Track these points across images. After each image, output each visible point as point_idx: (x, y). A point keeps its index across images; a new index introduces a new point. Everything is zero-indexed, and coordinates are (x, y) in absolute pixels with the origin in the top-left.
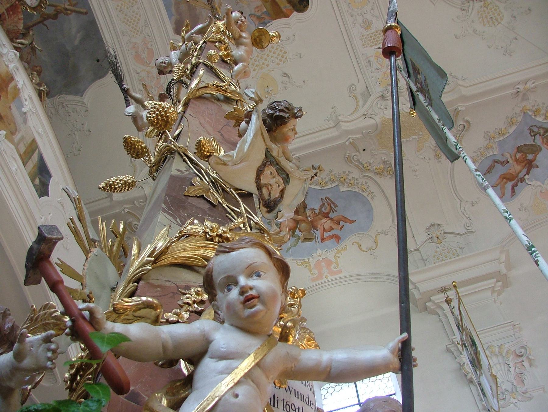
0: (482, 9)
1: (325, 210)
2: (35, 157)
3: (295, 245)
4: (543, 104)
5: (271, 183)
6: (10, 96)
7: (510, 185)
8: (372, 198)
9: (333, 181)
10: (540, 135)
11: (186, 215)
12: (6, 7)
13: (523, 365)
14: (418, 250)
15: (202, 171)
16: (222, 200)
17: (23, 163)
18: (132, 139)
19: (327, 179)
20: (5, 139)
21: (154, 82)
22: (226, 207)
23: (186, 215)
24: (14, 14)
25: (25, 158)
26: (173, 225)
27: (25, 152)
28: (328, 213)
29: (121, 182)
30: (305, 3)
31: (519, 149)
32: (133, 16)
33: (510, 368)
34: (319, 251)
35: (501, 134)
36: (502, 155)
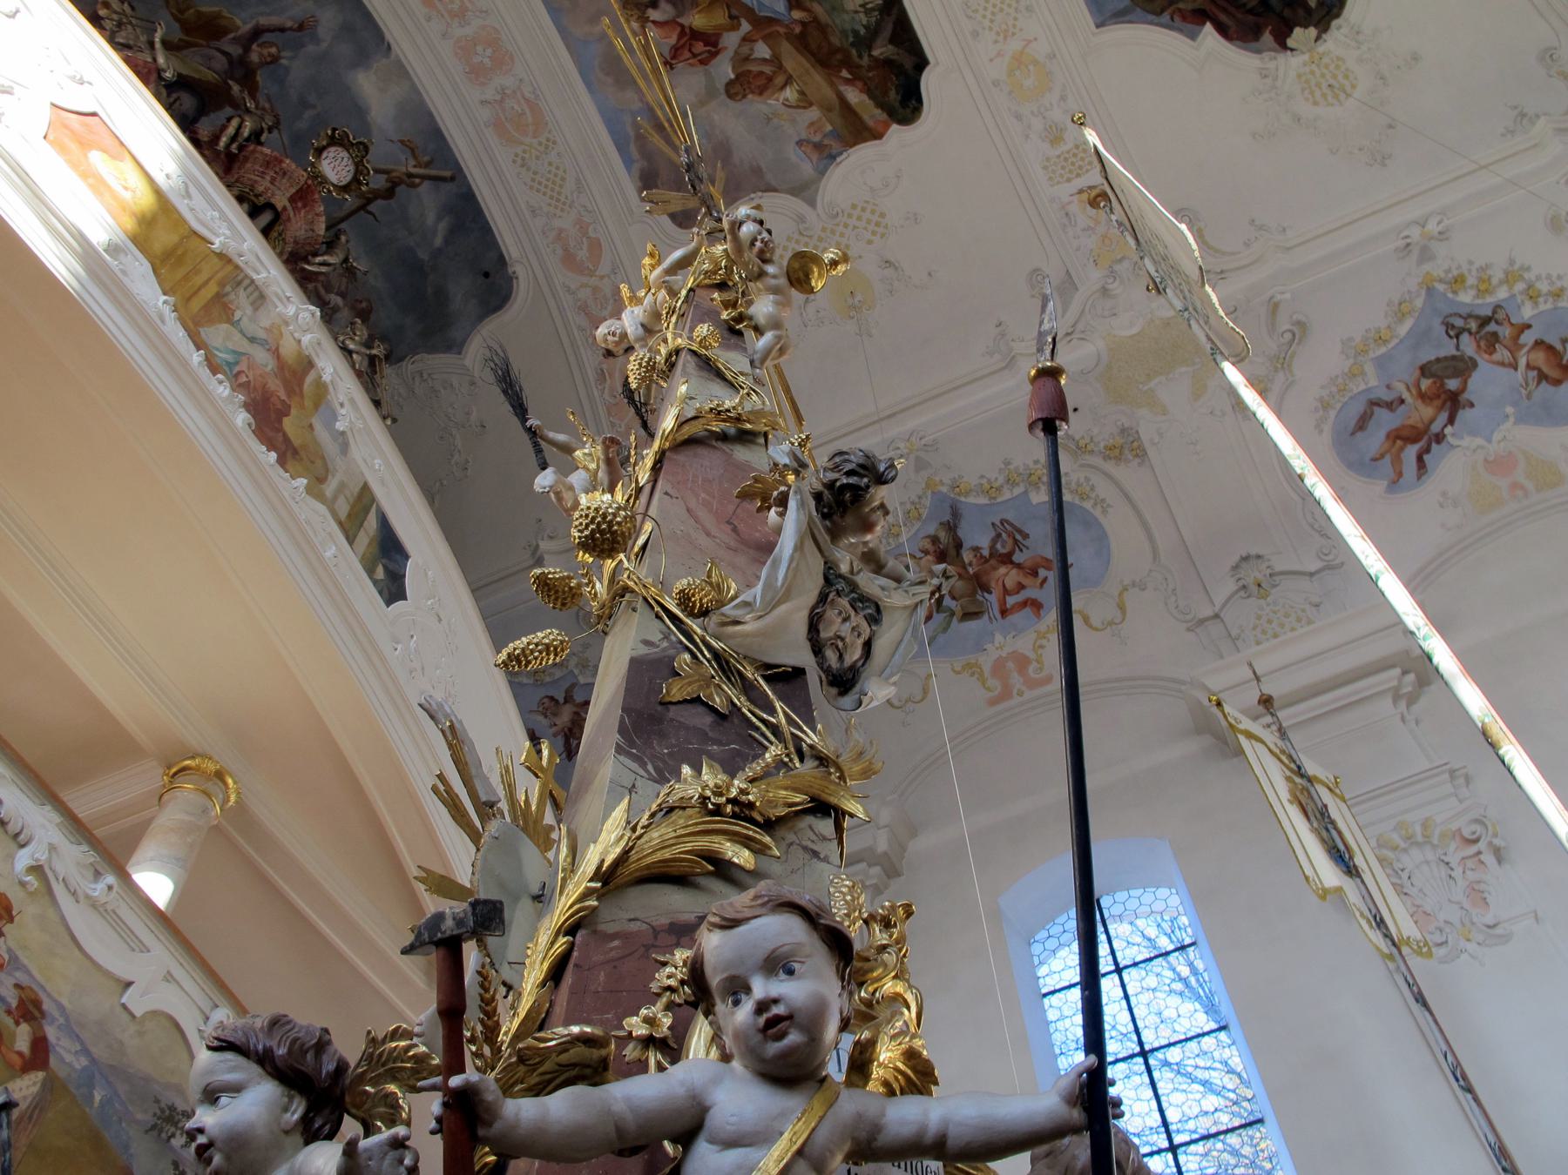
0: (1307, 69)
1: (1003, 546)
2: (372, 522)
3: (945, 630)
4: (1471, 263)
5: (843, 634)
6: (308, 403)
7: (1411, 451)
8: (1104, 511)
9: (1014, 484)
10: (1470, 333)
11: (666, 751)
12: (288, 195)
13: (1482, 863)
14: (1217, 616)
15: (696, 637)
16: (739, 700)
17: (347, 538)
18: (550, 576)
19: (1001, 480)
20: (308, 497)
21: (610, 308)
22: (749, 715)
23: (666, 751)
24: (305, 206)
25: (350, 529)
26: (639, 783)
27: (349, 516)
28: (1011, 554)
29: (540, 647)
30: (914, 102)
31: (1424, 370)
32: (549, 172)
33: (1452, 869)
34: (999, 638)
35: (1381, 341)
36: (1388, 387)
